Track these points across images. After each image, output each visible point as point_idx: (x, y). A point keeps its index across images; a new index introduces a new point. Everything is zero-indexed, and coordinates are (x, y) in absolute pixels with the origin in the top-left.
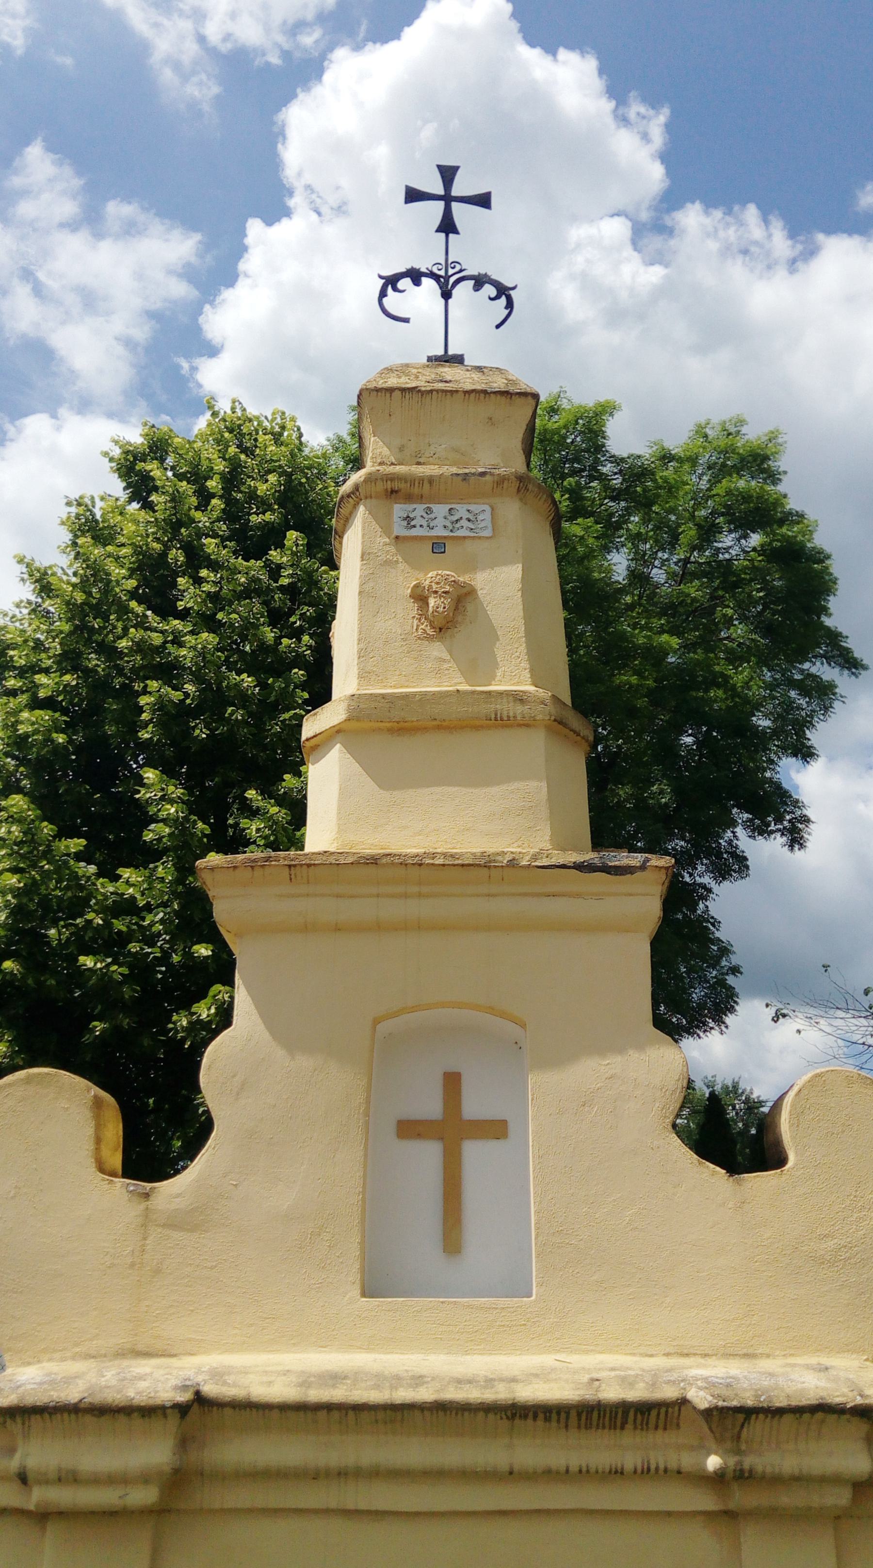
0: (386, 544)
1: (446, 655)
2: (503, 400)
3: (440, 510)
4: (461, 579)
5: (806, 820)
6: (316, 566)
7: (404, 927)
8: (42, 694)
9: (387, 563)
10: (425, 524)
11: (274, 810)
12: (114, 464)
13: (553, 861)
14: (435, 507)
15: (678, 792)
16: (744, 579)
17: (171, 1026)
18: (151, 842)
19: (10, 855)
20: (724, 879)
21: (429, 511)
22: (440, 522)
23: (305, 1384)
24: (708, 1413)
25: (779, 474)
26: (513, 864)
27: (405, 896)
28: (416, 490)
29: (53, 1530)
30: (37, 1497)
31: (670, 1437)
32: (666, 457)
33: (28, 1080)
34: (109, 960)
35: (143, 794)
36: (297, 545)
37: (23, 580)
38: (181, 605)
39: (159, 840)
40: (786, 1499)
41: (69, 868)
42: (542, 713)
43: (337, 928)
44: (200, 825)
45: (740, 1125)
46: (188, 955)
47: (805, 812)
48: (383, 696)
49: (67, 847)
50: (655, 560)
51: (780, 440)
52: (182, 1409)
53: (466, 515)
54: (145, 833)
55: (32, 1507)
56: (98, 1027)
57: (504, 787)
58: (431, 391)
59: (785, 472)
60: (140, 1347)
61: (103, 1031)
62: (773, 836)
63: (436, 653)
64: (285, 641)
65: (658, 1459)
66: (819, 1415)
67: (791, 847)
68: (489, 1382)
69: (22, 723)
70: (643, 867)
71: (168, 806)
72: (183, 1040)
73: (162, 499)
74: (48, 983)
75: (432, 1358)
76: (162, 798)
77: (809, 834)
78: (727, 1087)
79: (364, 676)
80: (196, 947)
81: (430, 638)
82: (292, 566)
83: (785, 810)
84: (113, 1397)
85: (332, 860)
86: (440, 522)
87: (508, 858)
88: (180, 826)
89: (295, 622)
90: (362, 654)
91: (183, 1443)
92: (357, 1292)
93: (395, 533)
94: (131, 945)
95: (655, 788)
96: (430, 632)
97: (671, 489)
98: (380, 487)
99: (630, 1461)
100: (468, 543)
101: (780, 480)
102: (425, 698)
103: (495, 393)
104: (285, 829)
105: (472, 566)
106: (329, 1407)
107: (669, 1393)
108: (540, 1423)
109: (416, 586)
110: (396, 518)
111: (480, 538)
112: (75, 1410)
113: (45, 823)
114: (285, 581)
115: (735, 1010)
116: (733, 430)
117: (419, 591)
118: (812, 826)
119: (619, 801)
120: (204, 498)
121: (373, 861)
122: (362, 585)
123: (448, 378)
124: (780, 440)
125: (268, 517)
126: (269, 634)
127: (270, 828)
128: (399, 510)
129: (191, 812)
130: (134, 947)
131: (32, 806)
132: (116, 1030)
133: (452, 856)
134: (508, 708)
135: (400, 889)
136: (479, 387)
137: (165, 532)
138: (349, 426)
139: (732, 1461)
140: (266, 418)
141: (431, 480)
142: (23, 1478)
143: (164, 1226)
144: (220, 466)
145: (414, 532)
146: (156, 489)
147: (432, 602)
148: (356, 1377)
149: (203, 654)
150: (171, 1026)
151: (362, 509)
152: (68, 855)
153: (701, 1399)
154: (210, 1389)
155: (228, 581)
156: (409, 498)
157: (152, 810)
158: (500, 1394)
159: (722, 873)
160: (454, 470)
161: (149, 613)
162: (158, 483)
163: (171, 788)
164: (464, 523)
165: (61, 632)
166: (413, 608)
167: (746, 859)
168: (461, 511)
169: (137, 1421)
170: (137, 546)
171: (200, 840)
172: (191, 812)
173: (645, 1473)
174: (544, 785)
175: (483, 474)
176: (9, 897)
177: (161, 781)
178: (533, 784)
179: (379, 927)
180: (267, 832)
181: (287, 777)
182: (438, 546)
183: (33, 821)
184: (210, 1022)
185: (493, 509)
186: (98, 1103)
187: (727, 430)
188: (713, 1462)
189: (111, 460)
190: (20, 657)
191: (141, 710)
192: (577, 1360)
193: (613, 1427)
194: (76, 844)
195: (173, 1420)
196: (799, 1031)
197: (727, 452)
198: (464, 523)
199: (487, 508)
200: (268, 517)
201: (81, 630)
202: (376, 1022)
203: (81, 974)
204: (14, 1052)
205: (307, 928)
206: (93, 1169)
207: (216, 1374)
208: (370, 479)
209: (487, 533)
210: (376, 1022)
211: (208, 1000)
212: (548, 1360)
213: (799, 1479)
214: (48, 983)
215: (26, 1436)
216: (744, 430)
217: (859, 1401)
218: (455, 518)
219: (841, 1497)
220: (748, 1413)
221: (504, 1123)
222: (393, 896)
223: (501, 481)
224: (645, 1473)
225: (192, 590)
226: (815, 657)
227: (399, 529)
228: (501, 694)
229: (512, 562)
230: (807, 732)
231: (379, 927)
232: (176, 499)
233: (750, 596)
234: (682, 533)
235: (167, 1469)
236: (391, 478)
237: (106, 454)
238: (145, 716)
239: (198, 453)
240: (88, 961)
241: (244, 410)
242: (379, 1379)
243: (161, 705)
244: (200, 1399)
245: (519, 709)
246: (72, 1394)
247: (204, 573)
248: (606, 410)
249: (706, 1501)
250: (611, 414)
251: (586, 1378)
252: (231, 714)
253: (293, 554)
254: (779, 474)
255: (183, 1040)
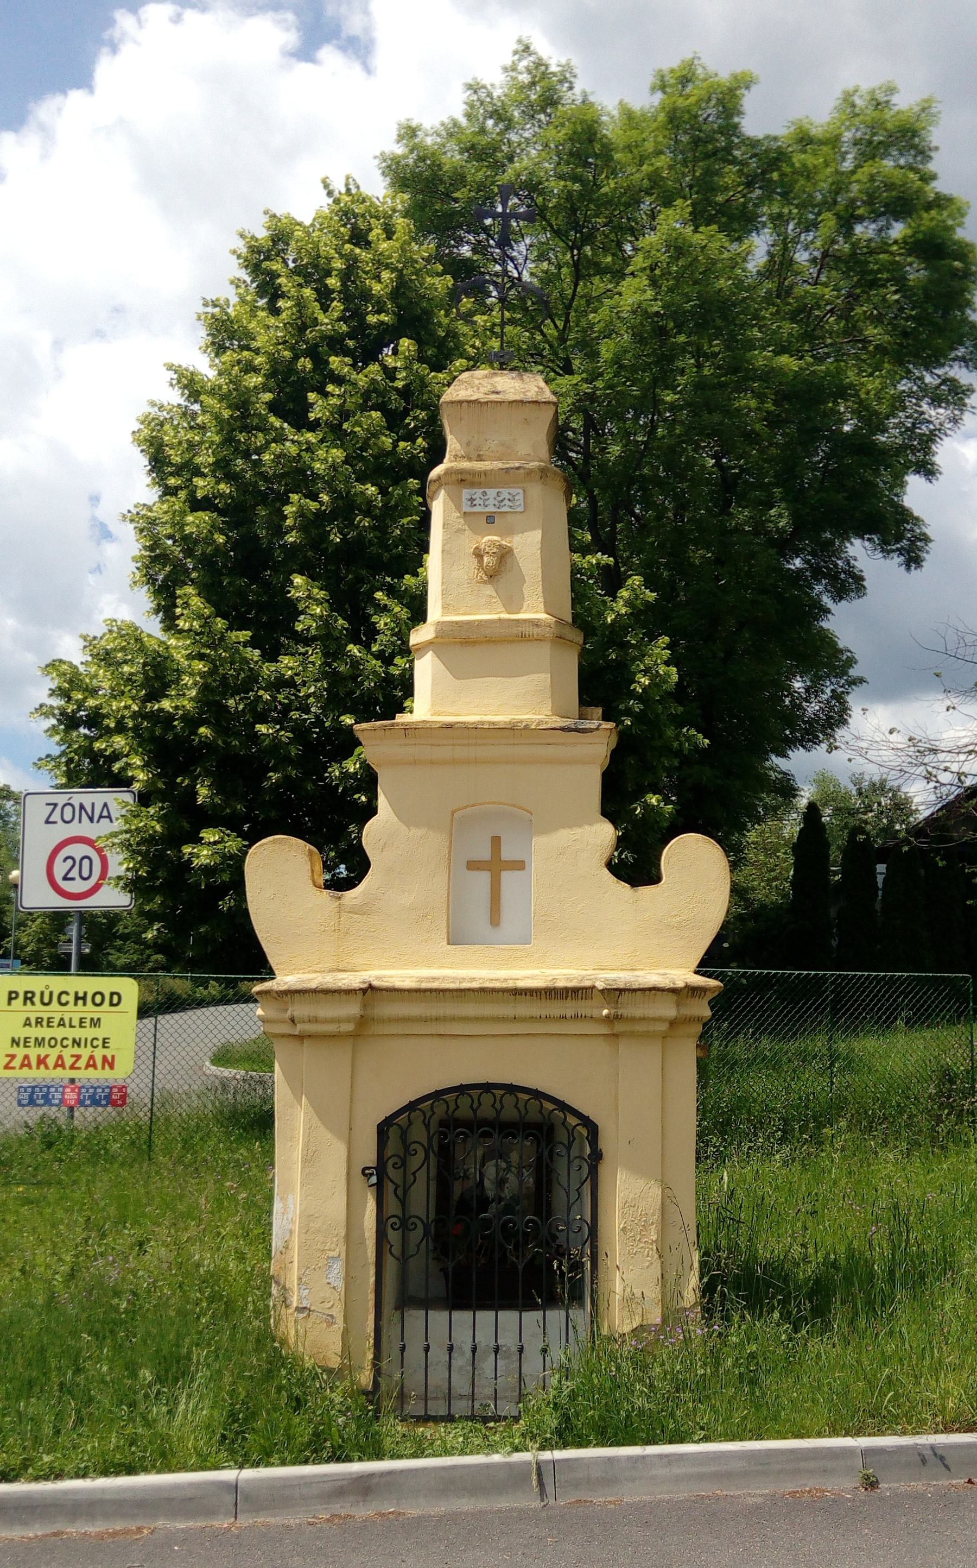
0: (458, 517)
1: (494, 594)
2: (534, 406)
3: (491, 493)
4: (504, 543)
5: (926, 539)
6: (426, 372)
7: (467, 762)
8: (199, 494)
9: (458, 531)
10: (482, 503)
11: (397, 609)
12: (241, 261)
13: (549, 726)
14: (489, 491)
15: (796, 517)
16: (880, 279)
17: (327, 775)
18: (302, 631)
19: (193, 644)
20: (841, 598)
21: (484, 493)
22: (491, 501)
23: (421, 981)
24: (602, 991)
25: (930, 149)
26: (527, 727)
27: (469, 745)
28: (477, 479)
29: (306, 1042)
30: (299, 1028)
31: (588, 1003)
32: (805, 140)
33: (274, 842)
34: (278, 727)
35: (294, 594)
36: (409, 351)
37: (171, 385)
38: (312, 416)
39: (308, 629)
40: (639, 1028)
41: (240, 654)
42: (548, 633)
43: (432, 762)
44: (341, 621)
45: (885, 821)
46: (336, 720)
47: (925, 530)
48: (457, 623)
49: (237, 637)
50: (797, 244)
51: (934, 110)
52: (364, 991)
53: (508, 497)
54: (297, 623)
55: (297, 1033)
56: (274, 776)
57: (524, 678)
58: (487, 402)
59: (937, 149)
60: (340, 968)
61: (277, 779)
62: (892, 554)
63: (488, 592)
64: (402, 444)
65: (582, 1012)
66: (653, 992)
67: (908, 568)
68: (506, 980)
69: (188, 525)
70: (597, 729)
71: (315, 607)
72: (337, 786)
73: (289, 304)
74: (233, 743)
75: (481, 971)
76: (309, 597)
77: (928, 552)
78: (874, 785)
79: (446, 608)
80: (342, 718)
81: (485, 582)
82: (405, 368)
83: (905, 528)
84: (331, 986)
85: (428, 725)
86: (491, 501)
87: (524, 724)
88: (326, 623)
89: (409, 424)
90: (445, 593)
91: (365, 1006)
92: (445, 943)
93: (464, 510)
94: (292, 713)
95: (773, 512)
96: (485, 578)
97: (808, 173)
98: (454, 477)
99: (569, 1013)
100: (509, 516)
101: (930, 157)
102: (481, 623)
103: (529, 402)
104: (405, 623)
105: (509, 531)
106: (431, 990)
107: (587, 983)
108: (528, 996)
109: (477, 548)
110: (464, 500)
111: (516, 512)
112: (315, 991)
113: (219, 619)
114: (400, 384)
115: (848, 723)
116: (882, 97)
117: (478, 552)
118: (930, 545)
119: (737, 524)
120: (324, 296)
121: (450, 726)
122: (444, 545)
123: (499, 389)
124: (934, 110)
125: (384, 318)
126: (387, 441)
127: (394, 622)
128: (466, 493)
129: (332, 611)
130: (295, 715)
131: (207, 605)
132: (287, 778)
133: (493, 723)
134: (529, 630)
135: (465, 742)
136: (518, 398)
137: (292, 336)
138: (465, 107)
139: (613, 1012)
140: (378, 199)
141: (485, 473)
142: (293, 1020)
143: (349, 912)
144: (338, 264)
145: (475, 509)
146: (283, 296)
147: (486, 559)
148: (444, 979)
149: (334, 467)
150: (327, 775)
151: (443, 492)
152: (239, 643)
153: (600, 985)
154: (376, 983)
155: (351, 395)
156: (472, 485)
157: (301, 606)
158: (510, 984)
159: (840, 593)
160: (500, 465)
161: (286, 425)
162: (285, 289)
163: (316, 591)
164: (506, 502)
165: (212, 443)
166: (475, 561)
167: (862, 579)
168: (505, 493)
169: (344, 997)
170: (269, 354)
171: (341, 631)
172: (332, 611)
173: (576, 1017)
174: (549, 675)
175: (518, 468)
176: (198, 679)
177: (307, 584)
178: (543, 676)
179: (454, 762)
180: (393, 625)
181: (407, 577)
182: (490, 519)
183: (209, 618)
184: (356, 773)
185: (524, 491)
186: (310, 853)
187: (876, 100)
188: (605, 1012)
189: (239, 257)
190: (176, 456)
191: (286, 517)
192: (549, 972)
193: (562, 998)
194: (244, 635)
195: (360, 994)
196: (850, 760)
197: (873, 128)
198: (506, 502)
199: (521, 491)
200: (384, 318)
201: (229, 440)
202: (453, 813)
203: (256, 737)
204: (213, 794)
205: (415, 763)
206: (312, 885)
207: (378, 978)
208: (448, 472)
209: (520, 509)
210: (453, 813)
211: (354, 758)
212: (537, 972)
213: (643, 1019)
214: (233, 743)
215: (292, 1003)
216: (895, 99)
217: (672, 986)
218: (500, 499)
219: (664, 1027)
220: (621, 991)
221: (523, 862)
222: (462, 745)
223: (530, 472)
224: (576, 1017)
225: (320, 402)
226: (954, 360)
227: (467, 508)
228: (525, 621)
229: (534, 529)
230: (933, 447)
231: (454, 762)
232: (300, 304)
233: (884, 300)
234: (821, 222)
235: (358, 1016)
236: (461, 472)
237: (234, 252)
238: (289, 522)
239: (316, 246)
240: (262, 729)
241: (358, 187)
242: (454, 979)
243: (301, 513)
244: (371, 987)
245: (536, 630)
246: (313, 985)
247: (330, 388)
248: (744, 82)
249: (605, 1030)
250: (748, 88)
251: (551, 978)
252: (360, 522)
253: (406, 358)
254: (930, 149)
255: (337, 786)
